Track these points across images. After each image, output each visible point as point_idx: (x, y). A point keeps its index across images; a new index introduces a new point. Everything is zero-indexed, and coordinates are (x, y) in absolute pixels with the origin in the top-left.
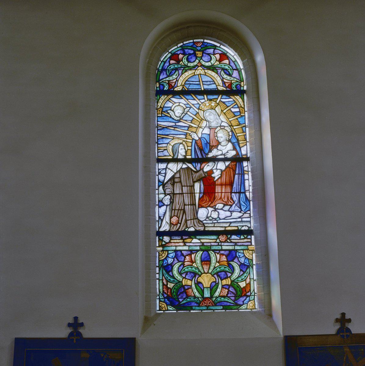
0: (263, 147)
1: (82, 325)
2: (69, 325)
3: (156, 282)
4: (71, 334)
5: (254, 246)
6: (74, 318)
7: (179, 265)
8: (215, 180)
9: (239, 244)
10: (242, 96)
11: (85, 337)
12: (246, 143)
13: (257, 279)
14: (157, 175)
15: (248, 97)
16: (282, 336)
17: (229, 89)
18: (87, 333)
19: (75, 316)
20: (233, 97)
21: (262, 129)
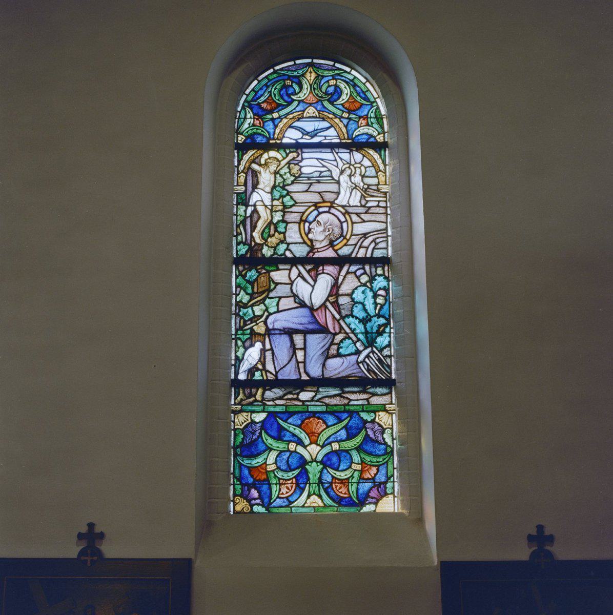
0: (412, 205)
1: (102, 536)
2: (80, 536)
3: (231, 432)
4: (82, 553)
5: (394, 406)
6: (87, 525)
7: (267, 436)
8: (328, 468)
9: (371, 360)
10: (383, 152)
11: (106, 557)
12: (387, 237)
13: (399, 436)
14: (235, 236)
15: (390, 153)
16: (436, 563)
17: (357, 501)
18: (111, 550)
19: (89, 521)
20: (367, 506)
21: (412, 212)
